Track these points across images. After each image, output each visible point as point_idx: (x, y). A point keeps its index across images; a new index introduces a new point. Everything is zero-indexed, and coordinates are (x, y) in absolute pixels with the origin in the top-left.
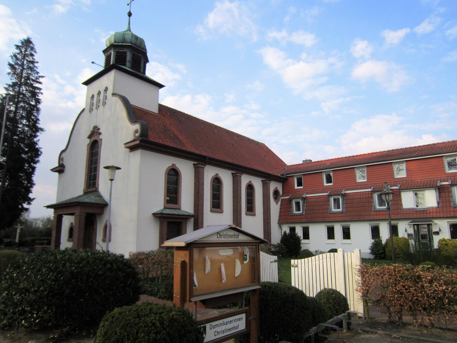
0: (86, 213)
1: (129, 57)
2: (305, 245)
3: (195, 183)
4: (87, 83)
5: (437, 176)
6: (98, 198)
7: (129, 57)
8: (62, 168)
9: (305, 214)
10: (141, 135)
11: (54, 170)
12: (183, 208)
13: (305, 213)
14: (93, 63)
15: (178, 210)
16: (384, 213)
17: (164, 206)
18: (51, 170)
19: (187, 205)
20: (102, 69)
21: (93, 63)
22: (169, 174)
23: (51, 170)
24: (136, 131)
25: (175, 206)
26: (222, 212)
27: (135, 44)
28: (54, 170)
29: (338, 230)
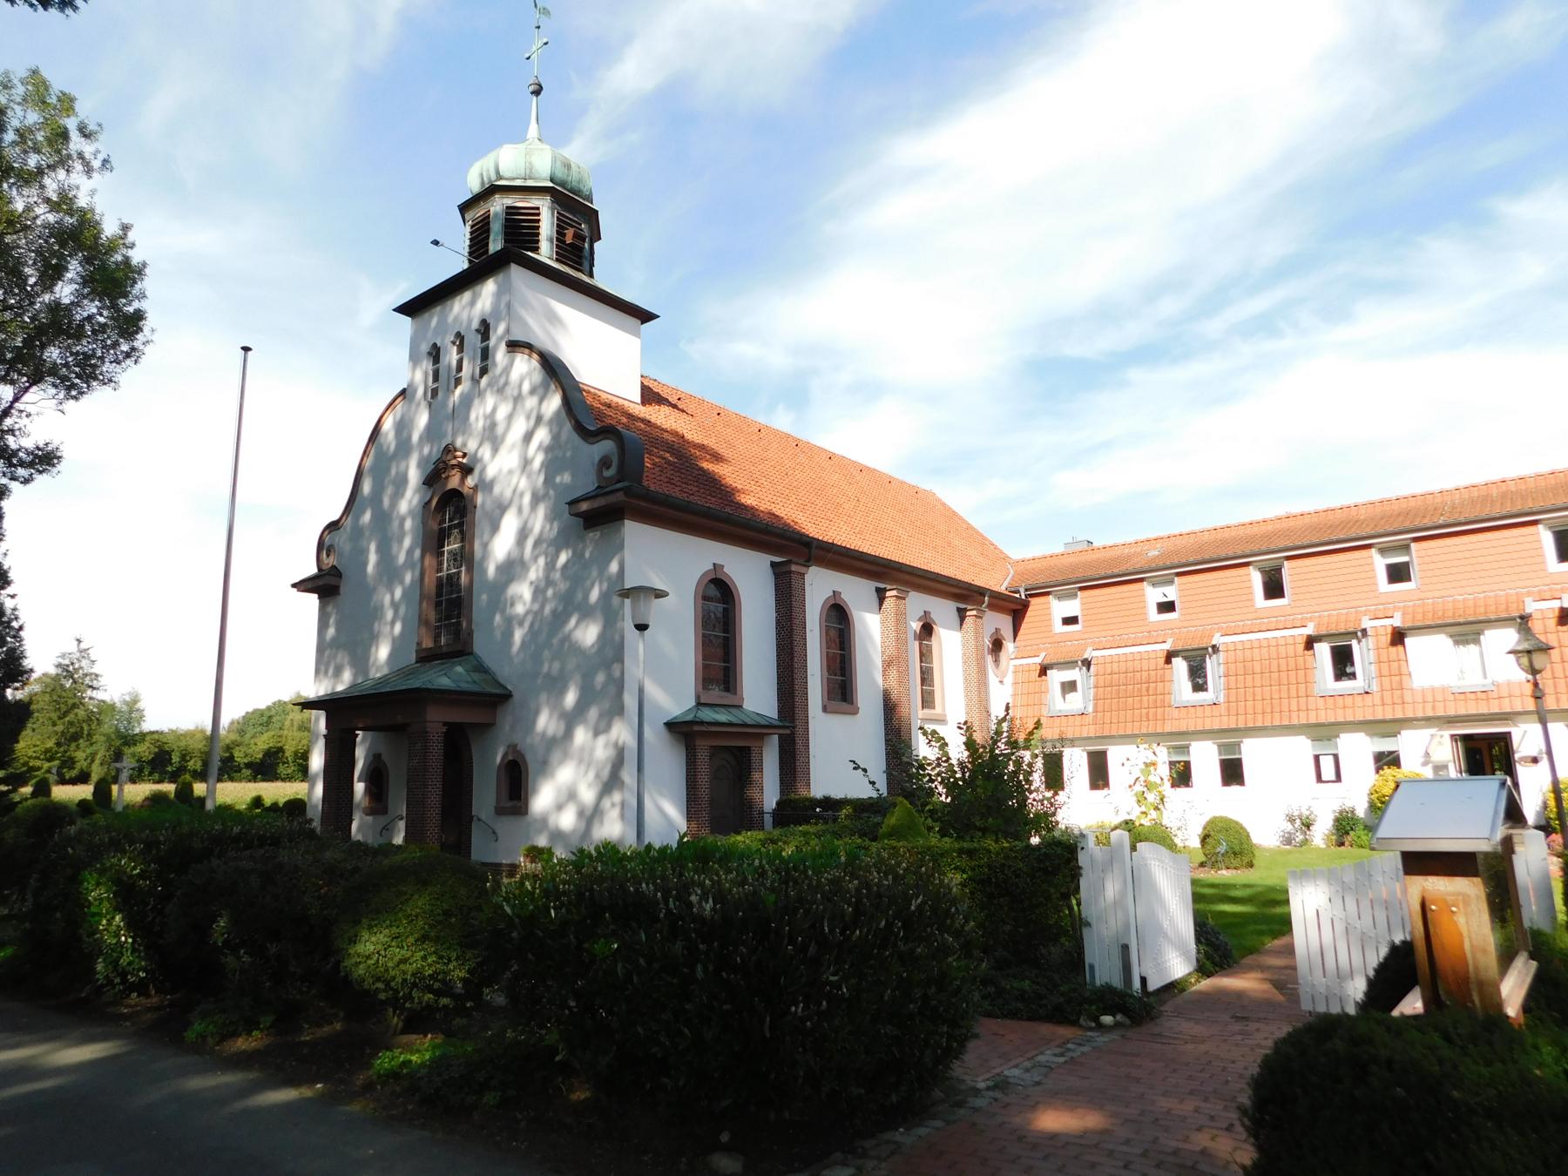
0: (445, 724)
1: (547, 226)
2: (225, 721)
3: (778, 622)
4: (413, 308)
5: (1486, 588)
6: (476, 676)
7: (547, 226)
8: (332, 581)
9: (1096, 711)
10: (622, 475)
11: (303, 586)
12: (748, 705)
13: (1095, 706)
14: (436, 243)
15: (734, 711)
16: (1349, 700)
17: (698, 697)
18: (294, 586)
19: (758, 694)
20: (460, 264)
21: (436, 243)
22: (705, 598)
23: (294, 586)
24: (605, 463)
25: (728, 699)
26: (855, 712)
27: (563, 184)
28: (303, 586)
29: (1205, 759)
